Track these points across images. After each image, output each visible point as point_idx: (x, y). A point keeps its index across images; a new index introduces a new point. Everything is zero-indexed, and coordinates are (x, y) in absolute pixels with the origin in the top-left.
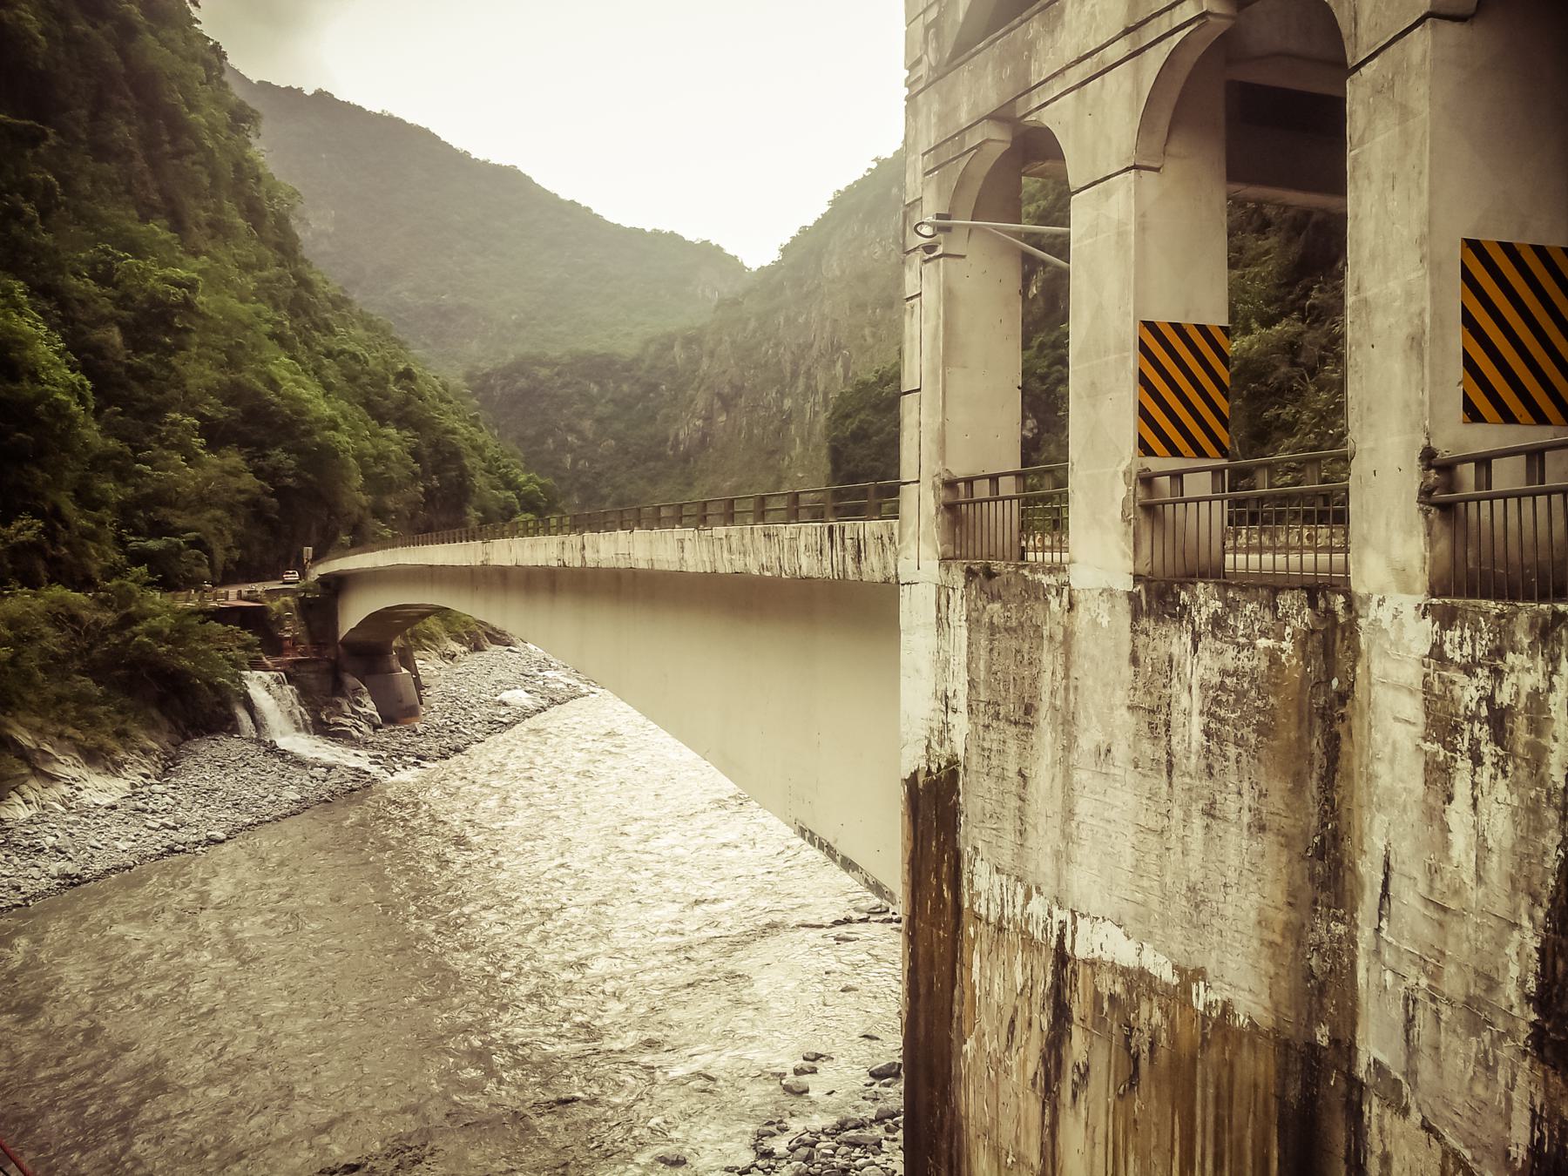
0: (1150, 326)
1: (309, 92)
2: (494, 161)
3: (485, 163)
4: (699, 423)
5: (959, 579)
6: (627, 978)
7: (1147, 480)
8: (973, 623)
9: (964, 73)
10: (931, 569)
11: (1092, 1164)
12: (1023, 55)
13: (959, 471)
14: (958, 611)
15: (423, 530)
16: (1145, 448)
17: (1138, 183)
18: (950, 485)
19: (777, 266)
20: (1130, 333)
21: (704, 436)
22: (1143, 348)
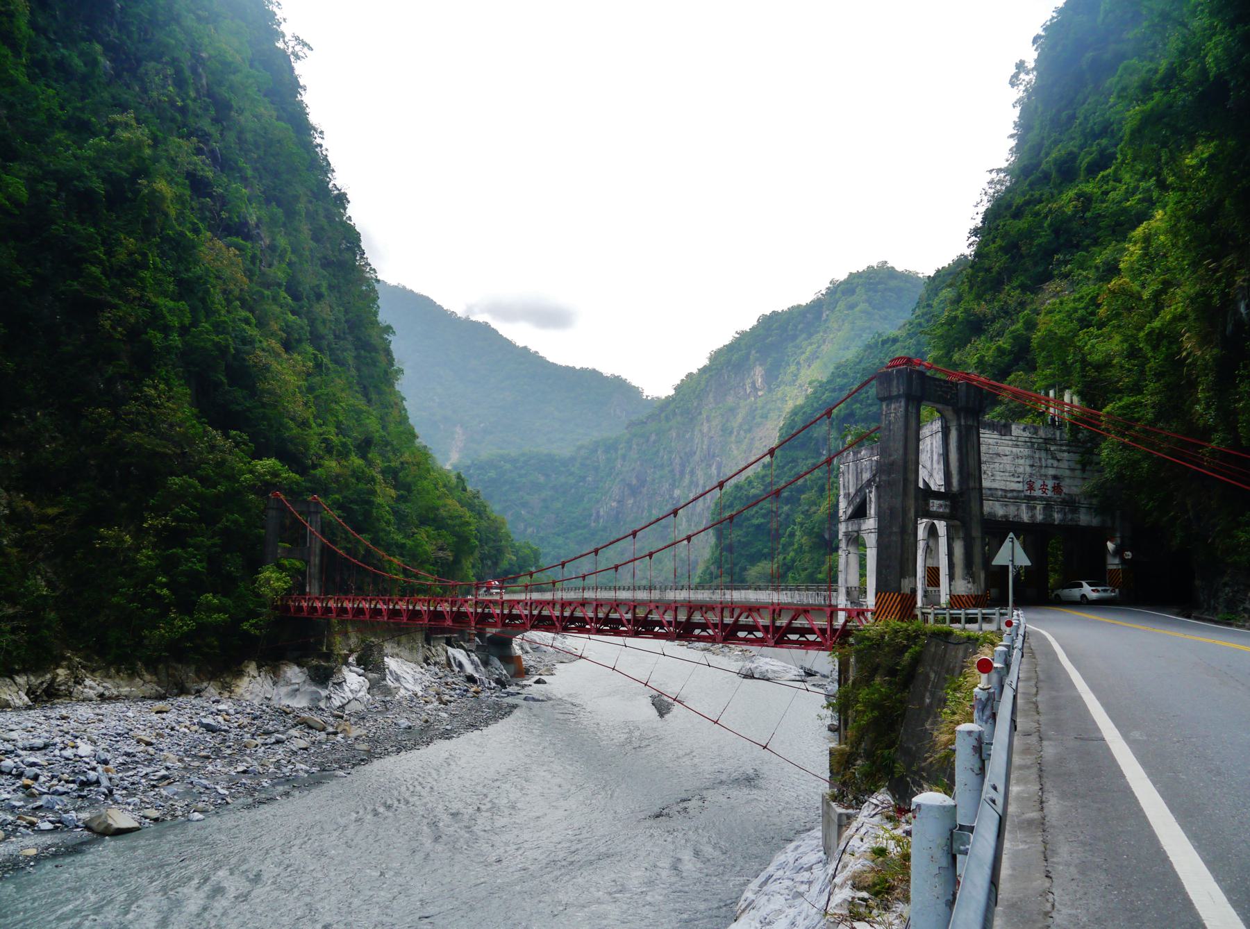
4: (614, 504)
19: (669, 400)
21: (618, 513)
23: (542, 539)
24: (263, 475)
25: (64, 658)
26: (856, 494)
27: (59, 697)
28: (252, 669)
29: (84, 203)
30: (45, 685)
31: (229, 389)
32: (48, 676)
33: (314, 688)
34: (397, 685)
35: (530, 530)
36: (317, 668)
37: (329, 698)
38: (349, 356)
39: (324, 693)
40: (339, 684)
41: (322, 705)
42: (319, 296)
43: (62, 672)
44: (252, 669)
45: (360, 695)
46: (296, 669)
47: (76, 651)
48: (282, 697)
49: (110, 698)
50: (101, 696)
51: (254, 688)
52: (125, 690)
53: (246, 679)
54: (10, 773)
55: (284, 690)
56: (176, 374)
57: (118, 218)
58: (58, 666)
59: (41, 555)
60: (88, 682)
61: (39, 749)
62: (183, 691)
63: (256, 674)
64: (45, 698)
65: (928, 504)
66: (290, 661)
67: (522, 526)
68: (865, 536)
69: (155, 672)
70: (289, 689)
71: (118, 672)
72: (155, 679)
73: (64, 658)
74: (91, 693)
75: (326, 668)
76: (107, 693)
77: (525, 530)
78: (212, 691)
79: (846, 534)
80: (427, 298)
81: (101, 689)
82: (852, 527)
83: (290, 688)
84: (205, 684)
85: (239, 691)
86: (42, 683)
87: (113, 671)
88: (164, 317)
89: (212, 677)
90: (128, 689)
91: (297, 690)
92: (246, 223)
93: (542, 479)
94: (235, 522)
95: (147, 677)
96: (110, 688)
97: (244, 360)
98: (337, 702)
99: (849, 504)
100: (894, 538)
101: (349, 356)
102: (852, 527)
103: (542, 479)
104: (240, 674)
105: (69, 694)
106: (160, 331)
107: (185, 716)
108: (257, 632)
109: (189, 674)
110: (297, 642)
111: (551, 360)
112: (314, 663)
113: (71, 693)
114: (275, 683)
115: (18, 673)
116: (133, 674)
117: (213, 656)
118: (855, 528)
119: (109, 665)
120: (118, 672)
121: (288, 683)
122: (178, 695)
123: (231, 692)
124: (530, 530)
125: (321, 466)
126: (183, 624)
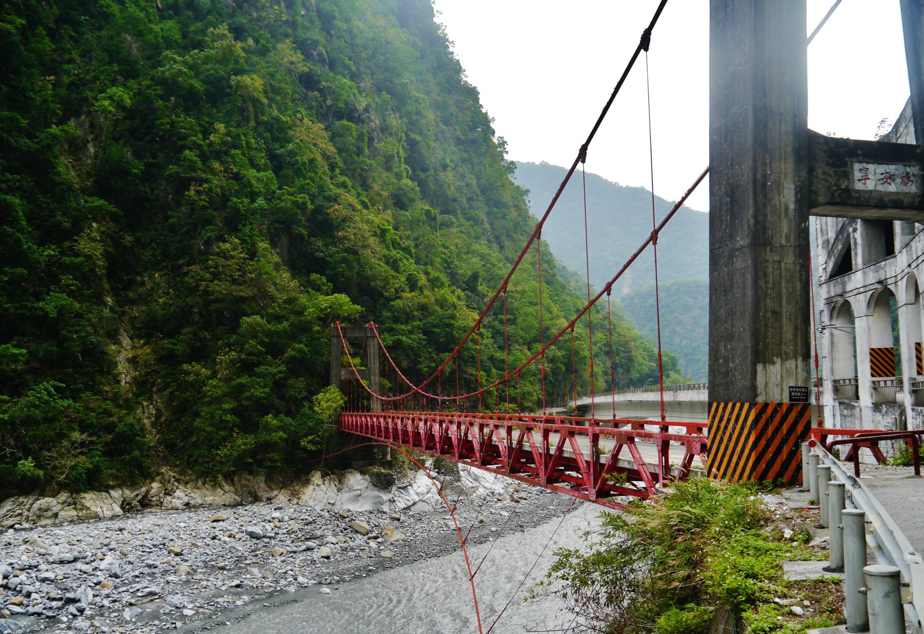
0: (872, 349)
1: (484, 111)
2: (632, 185)
3: (627, 187)
5: (837, 404)
6: (367, 83)
7: (874, 382)
8: (841, 415)
9: (832, 283)
10: (831, 400)
11: (817, 366)
12: (844, 284)
13: (837, 378)
14: (838, 414)
15: (608, 391)
16: (873, 375)
17: (868, 320)
18: (835, 381)
20: (868, 351)
22: (871, 354)
23: (694, 348)
24: (326, 309)
25: (158, 474)
26: (836, 239)
27: (151, 506)
28: (316, 478)
29: (190, 101)
30: (140, 497)
31: (311, 241)
32: (144, 489)
33: (376, 493)
34: (476, 484)
35: (684, 342)
36: (378, 475)
37: (392, 501)
38: (481, 214)
39: (386, 497)
40: (404, 488)
41: (385, 508)
42: (445, 167)
43: (155, 485)
44: (316, 478)
45: (427, 497)
46: (358, 476)
47: (173, 466)
48: (344, 503)
49: (194, 506)
50: (187, 504)
51: (319, 494)
52: (209, 499)
53: (311, 487)
54: (15, 590)
55: (345, 495)
56: (261, 232)
57: (219, 112)
58: (153, 480)
59: (155, 389)
60: (178, 493)
61: (69, 562)
62: (256, 499)
63: (320, 482)
64: (139, 508)
65: (847, 175)
66: (355, 469)
67: (678, 340)
68: (852, 300)
69: (232, 483)
70: (354, 495)
71: (204, 484)
72: (232, 489)
73: (158, 474)
74: (178, 503)
75: (386, 475)
76: (192, 502)
77: (681, 342)
78: (282, 498)
79: (829, 301)
80: (596, 175)
81: (186, 499)
82: (835, 289)
83: (352, 494)
84: (275, 492)
85: (304, 498)
86: (137, 495)
87: (200, 483)
88: (251, 185)
89: (283, 486)
90: (212, 498)
91: (360, 495)
92: (355, 109)
93: (691, 302)
94: (301, 351)
95: (227, 488)
96: (197, 497)
97: (327, 214)
98: (401, 504)
99: (829, 256)
100: (739, 264)
101: (481, 214)
102: (835, 289)
103: (691, 302)
104: (307, 482)
105: (160, 504)
106: (246, 197)
107: (261, 517)
108: (313, 448)
109: (259, 483)
110: (353, 452)
111: (623, 183)
112: (376, 470)
113: (162, 503)
114: (339, 490)
115: (113, 488)
116: (216, 485)
117: (289, 467)
118: (839, 291)
119: (199, 477)
120: (204, 484)
121: (350, 490)
122: (252, 503)
123: (299, 499)
124: (684, 342)
125: (400, 298)
126: (244, 442)
